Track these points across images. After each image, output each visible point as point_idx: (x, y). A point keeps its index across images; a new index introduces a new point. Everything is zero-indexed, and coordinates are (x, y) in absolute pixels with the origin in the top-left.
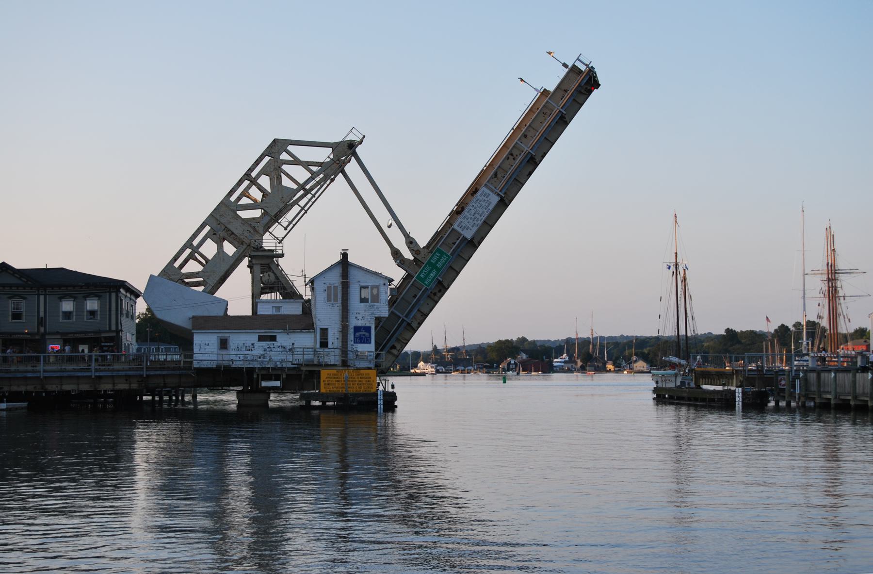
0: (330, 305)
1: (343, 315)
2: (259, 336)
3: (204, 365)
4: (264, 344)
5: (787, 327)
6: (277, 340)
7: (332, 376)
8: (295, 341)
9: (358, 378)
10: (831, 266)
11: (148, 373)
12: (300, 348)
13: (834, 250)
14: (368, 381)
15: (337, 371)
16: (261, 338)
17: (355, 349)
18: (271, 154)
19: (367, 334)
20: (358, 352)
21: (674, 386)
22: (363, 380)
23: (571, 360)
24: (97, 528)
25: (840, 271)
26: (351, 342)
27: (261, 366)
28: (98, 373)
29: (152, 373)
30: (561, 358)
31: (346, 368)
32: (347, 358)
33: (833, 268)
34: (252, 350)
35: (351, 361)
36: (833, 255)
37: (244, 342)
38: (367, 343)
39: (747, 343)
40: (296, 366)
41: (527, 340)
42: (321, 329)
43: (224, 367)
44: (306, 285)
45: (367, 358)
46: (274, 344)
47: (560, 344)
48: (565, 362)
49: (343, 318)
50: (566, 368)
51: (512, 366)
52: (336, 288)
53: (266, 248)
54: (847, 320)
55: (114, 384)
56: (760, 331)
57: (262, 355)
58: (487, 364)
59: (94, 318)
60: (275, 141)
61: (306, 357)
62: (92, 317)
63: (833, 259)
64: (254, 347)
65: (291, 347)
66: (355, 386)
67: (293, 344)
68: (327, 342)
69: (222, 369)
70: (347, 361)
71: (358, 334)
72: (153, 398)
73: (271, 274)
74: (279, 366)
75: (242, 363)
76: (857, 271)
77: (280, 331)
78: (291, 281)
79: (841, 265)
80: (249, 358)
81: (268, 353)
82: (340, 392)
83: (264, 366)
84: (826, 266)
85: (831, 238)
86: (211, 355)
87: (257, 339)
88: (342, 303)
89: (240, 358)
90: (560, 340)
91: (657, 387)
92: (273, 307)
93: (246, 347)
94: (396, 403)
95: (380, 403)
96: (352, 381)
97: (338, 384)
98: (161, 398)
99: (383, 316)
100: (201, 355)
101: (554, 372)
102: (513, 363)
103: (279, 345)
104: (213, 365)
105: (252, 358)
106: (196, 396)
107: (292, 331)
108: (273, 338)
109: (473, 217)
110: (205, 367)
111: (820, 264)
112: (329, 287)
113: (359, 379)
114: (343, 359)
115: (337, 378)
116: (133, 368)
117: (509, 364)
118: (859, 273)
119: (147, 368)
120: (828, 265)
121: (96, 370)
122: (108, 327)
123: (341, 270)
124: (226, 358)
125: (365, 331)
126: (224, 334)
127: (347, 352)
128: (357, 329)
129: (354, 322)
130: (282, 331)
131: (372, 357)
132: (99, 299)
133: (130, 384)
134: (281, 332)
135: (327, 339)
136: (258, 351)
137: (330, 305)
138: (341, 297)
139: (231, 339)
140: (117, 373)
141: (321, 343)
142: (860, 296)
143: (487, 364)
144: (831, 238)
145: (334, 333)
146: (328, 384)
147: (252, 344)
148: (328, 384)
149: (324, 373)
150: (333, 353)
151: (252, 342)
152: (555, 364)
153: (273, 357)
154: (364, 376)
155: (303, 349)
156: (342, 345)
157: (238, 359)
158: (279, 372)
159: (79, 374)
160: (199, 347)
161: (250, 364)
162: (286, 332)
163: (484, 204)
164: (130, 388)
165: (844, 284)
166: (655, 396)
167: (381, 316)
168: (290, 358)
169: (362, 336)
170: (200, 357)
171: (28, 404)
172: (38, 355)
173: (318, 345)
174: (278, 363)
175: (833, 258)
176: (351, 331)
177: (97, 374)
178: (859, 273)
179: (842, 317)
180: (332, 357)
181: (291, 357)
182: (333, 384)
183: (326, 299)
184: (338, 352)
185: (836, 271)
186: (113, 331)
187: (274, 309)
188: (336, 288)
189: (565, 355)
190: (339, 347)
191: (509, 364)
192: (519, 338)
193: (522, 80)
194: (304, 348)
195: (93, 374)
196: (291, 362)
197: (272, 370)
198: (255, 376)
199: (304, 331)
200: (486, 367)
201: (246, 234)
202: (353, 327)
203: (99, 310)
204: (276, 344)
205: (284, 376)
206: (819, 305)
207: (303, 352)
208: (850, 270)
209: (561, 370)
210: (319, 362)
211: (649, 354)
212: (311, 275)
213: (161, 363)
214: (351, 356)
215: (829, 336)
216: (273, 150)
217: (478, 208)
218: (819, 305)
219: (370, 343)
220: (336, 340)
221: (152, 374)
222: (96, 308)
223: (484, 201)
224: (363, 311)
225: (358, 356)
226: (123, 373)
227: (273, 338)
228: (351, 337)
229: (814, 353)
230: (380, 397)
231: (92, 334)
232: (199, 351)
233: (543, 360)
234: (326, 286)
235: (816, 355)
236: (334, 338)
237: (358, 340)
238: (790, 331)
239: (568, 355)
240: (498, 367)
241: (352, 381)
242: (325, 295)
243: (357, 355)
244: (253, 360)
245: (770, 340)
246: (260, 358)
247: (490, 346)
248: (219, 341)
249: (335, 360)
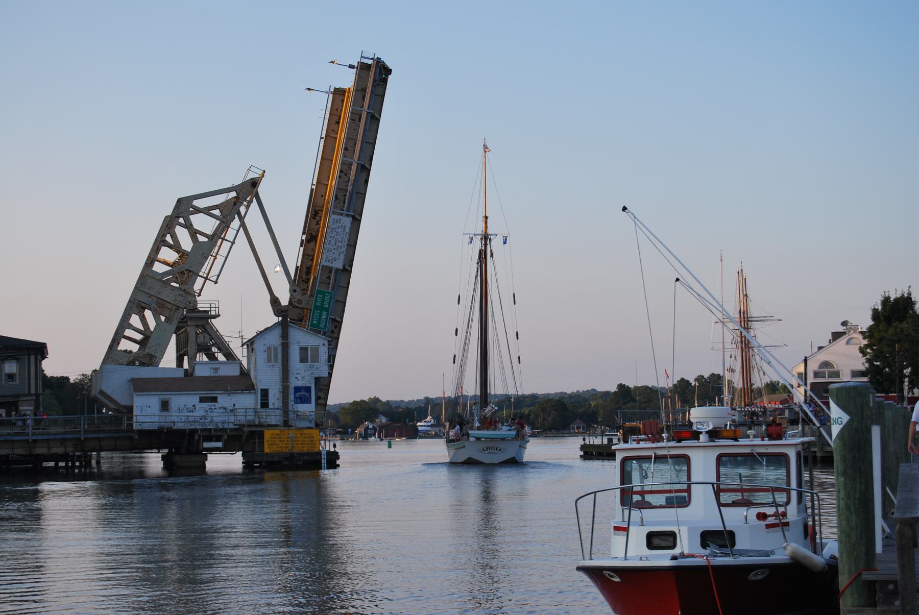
0: (270, 366)
1: (283, 375)
2: (200, 397)
3: (146, 427)
4: (206, 405)
5: (688, 381)
6: (218, 401)
7: (275, 436)
8: (236, 402)
9: (301, 437)
10: (744, 313)
11: (85, 436)
12: (243, 409)
13: (746, 295)
14: (312, 441)
15: (281, 432)
16: (202, 400)
17: (296, 409)
18: (179, 214)
19: (307, 394)
20: (299, 412)
21: (601, 443)
22: (307, 439)
23: (438, 423)
24: (129, 572)
25: (753, 319)
26: (291, 403)
27: (202, 428)
28: (35, 436)
29: (90, 436)
30: (425, 422)
31: (288, 428)
32: (288, 417)
33: (745, 316)
34: (193, 412)
35: (292, 421)
36: (745, 301)
37: (185, 404)
38: (307, 403)
39: (643, 400)
40: (237, 427)
41: (380, 401)
42: (262, 390)
43: (167, 428)
44: (243, 345)
45: (308, 418)
46: (215, 405)
47: (419, 406)
48: (432, 426)
49: (283, 378)
50: (433, 433)
51: (371, 431)
52: (275, 349)
53: (201, 309)
54: (761, 373)
55: (49, 448)
56: (652, 386)
57: (203, 416)
58: (340, 430)
59: (12, 381)
60: (179, 201)
61: (248, 418)
62: (10, 380)
63: (745, 306)
64: (195, 409)
65: (232, 408)
66: (298, 446)
67: (234, 405)
68: (268, 403)
69: (165, 431)
70: (288, 421)
71: (298, 394)
72: (56, 464)
73: (206, 335)
74: (220, 427)
75: (183, 424)
76: (772, 318)
77: (221, 392)
78: (226, 342)
79: (754, 312)
80: (190, 419)
81: (209, 414)
82: (284, 452)
83: (205, 427)
84: (738, 313)
85: (742, 281)
86: (152, 417)
87: (198, 401)
88: (282, 364)
89: (181, 419)
90: (415, 400)
91: (584, 444)
92: (211, 368)
93: (188, 408)
94: (338, 462)
95: (324, 461)
96: (296, 441)
97: (282, 444)
98: (73, 464)
99: (323, 376)
100: (143, 417)
101: (421, 437)
102: (372, 427)
103: (220, 406)
104: (155, 427)
105: (194, 419)
106: (100, 461)
107: (233, 392)
108: (214, 400)
109: (336, 247)
110: (147, 429)
111: (733, 310)
112: (269, 348)
113: (303, 439)
114: (285, 419)
115: (281, 438)
116: (68, 431)
117: (367, 429)
118: (774, 320)
119: (84, 431)
120: (740, 312)
121: (34, 434)
122: (27, 389)
123: (281, 330)
124: (168, 419)
125: (305, 391)
126: (165, 396)
127: (288, 412)
128: (297, 389)
129: (294, 382)
130: (224, 392)
131: (312, 417)
132: (17, 362)
133: (65, 448)
134: (223, 393)
135: (268, 400)
136: (199, 413)
137: (270, 366)
138: (281, 358)
139: (172, 401)
140: (54, 436)
141: (262, 404)
142: (775, 346)
143: (340, 430)
144: (742, 281)
145: (275, 394)
146: (272, 444)
147: (194, 406)
148: (272, 444)
149: (268, 434)
150: (273, 414)
151: (194, 404)
152: (420, 429)
153: (215, 419)
154: (308, 435)
155: (246, 410)
156: (283, 405)
157: (179, 420)
158: (221, 433)
159: (16, 438)
160: (140, 409)
161: (191, 425)
162: (227, 393)
163: (339, 230)
164: (65, 452)
165: (758, 333)
166: (582, 453)
167: (321, 376)
168: (232, 419)
169: (302, 396)
170: (141, 419)
171: (55, 464)
172: (9, 418)
173: (259, 406)
174: (219, 424)
175: (745, 304)
176: (292, 391)
177: (34, 438)
178: (774, 320)
179: (756, 370)
180: (273, 417)
181: (233, 418)
182: (277, 444)
183: (266, 360)
184: (278, 412)
185: (749, 319)
186: (33, 395)
187: (212, 370)
188: (275, 349)
189: (429, 418)
190: (279, 407)
191: (367, 429)
192: (370, 398)
193: (309, 89)
194: (246, 409)
195: (31, 438)
196: (233, 423)
197: (200, 431)
198: (196, 437)
199: (245, 392)
200: (339, 433)
201: (179, 298)
202: (293, 387)
203: (18, 374)
204: (217, 405)
205: (226, 437)
206: (731, 357)
207: (246, 412)
208: (765, 317)
209: (427, 435)
210: (260, 423)
211: (529, 415)
212: (249, 335)
213: (96, 426)
214: (291, 415)
215: (743, 391)
216: (180, 210)
217: (336, 237)
218: (731, 357)
219: (310, 403)
220: (277, 401)
221: (89, 437)
222: (15, 371)
223: (339, 227)
224: (303, 372)
225: (298, 416)
226: (61, 437)
227: (214, 400)
228: (292, 397)
229: (741, 408)
230: (324, 457)
231: (11, 398)
232: (141, 412)
233: (405, 424)
234: (266, 347)
235: (743, 410)
236: (274, 398)
237: (298, 400)
238: (691, 386)
239: (433, 418)
240: (353, 432)
241: (296, 441)
242: (265, 355)
243: (297, 415)
244: (194, 422)
245: (670, 397)
246: (201, 419)
247: (343, 409)
248: (161, 403)
249: (276, 420)
